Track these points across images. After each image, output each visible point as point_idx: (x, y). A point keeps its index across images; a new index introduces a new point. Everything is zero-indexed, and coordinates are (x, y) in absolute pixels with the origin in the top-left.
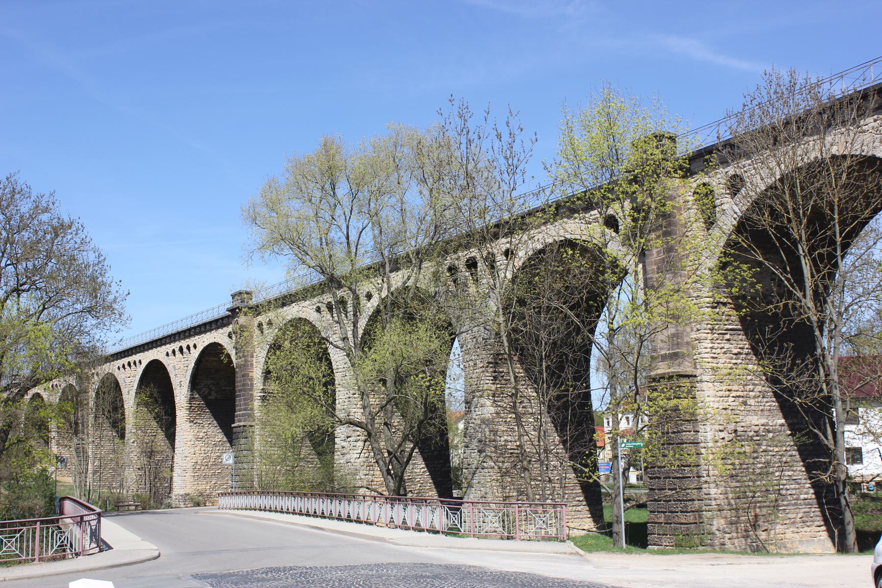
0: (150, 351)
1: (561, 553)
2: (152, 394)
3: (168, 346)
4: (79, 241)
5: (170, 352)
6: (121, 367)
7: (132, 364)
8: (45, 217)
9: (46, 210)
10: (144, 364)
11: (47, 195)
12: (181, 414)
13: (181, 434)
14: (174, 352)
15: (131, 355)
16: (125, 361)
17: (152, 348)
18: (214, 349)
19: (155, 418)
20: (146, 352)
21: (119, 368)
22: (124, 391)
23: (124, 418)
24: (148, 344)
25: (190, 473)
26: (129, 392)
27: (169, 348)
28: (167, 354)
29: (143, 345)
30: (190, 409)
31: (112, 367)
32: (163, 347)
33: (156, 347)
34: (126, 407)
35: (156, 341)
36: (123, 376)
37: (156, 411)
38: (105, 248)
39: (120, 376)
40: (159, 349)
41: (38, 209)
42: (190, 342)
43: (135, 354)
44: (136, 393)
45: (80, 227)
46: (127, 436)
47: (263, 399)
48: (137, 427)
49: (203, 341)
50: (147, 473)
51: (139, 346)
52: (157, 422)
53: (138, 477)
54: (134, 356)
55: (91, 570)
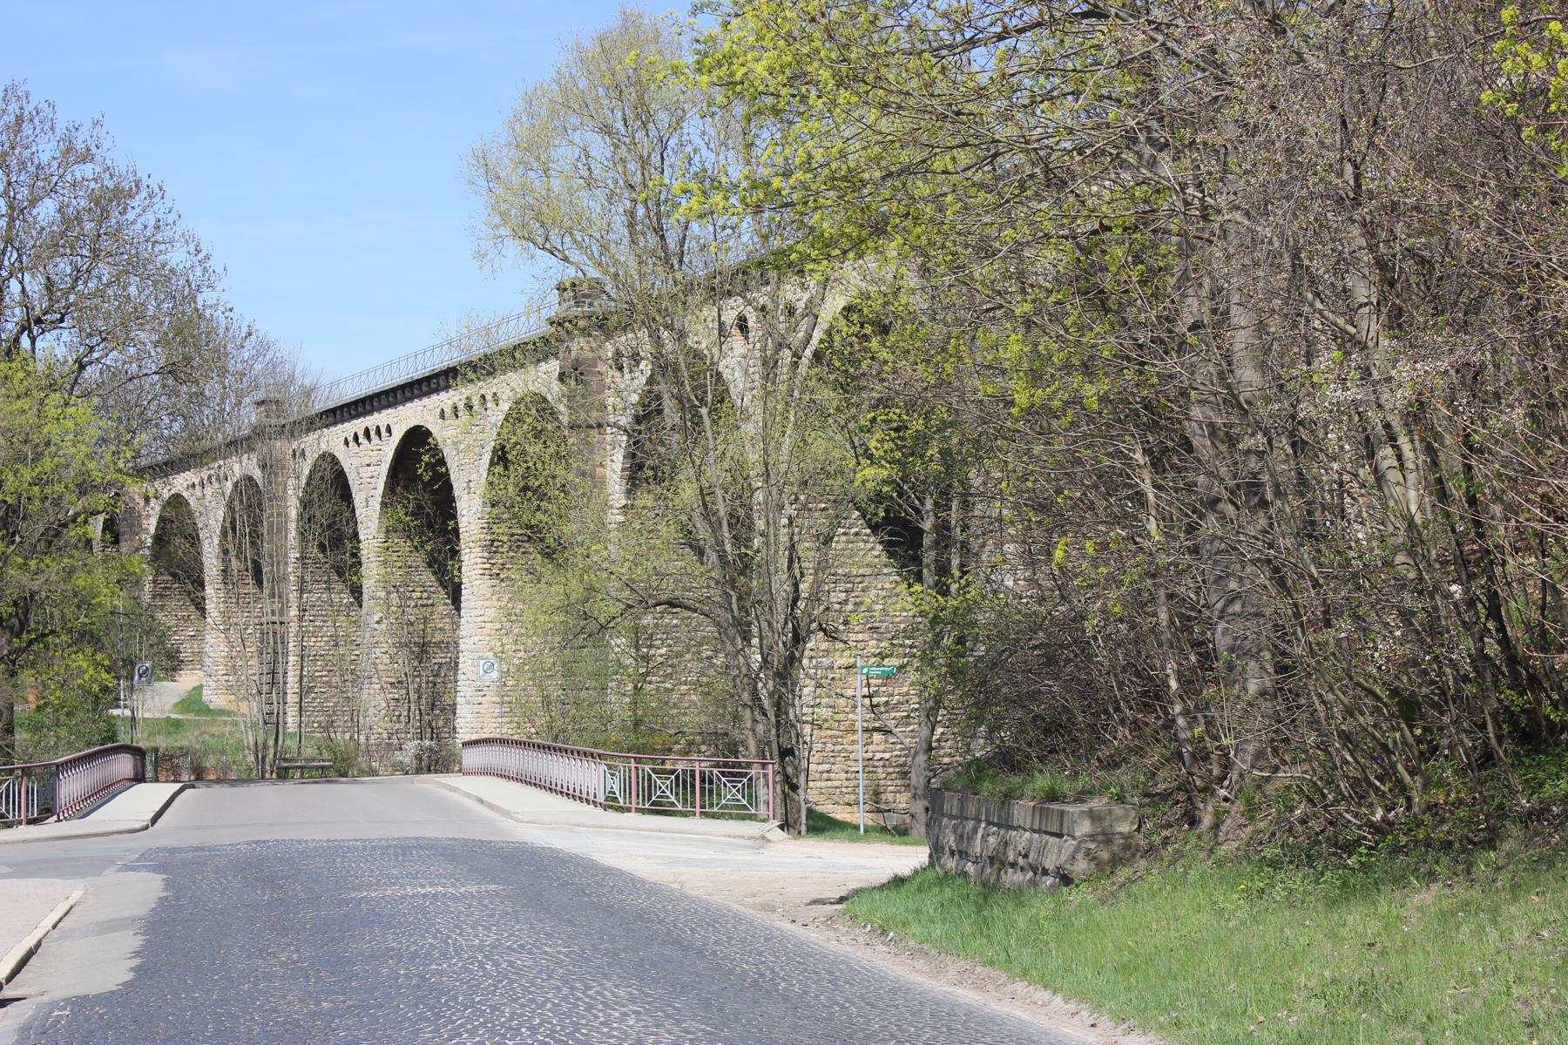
0: (409, 405)
1: (735, 837)
2: (420, 507)
3: (443, 395)
4: (152, 223)
5: (448, 411)
6: (350, 439)
7: (373, 433)
8: (88, 170)
9: (86, 157)
10: (398, 434)
11: (88, 125)
12: (472, 562)
13: (472, 604)
14: (356, 438)
15: (370, 412)
16: (358, 425)
17: (411, 399)
18: (417, 437)
19: (430, 565)
20: (400, 408)
21: (347, 443)
22: (358, 499)
23: (360, 564)
24: (402, 387)
25: (491, 697)
26: (367, 501)
27: (445, 399)
28: (442, 415)
29: (394, 390)
30: (492, 547)
31: (333, 439)
32: (434, 397)
33: (420, 397)
34: (362, 537)
35: (419, 382)
36: (356, 461)
37: (428, 548)
38: (209, 233)
39: (350, 461)
40: (425, 400)
41: (73, 154)
42: (488, 387)
43: (379, 410)
44: (384, 505)
45: (157, 190)
46: (365, 597)
47: (1157, 465)
48: (390, 587)
49: (402, 418)
50: (413, 696)
51: (386, 393)
52: (434, 573)
53: (393, 703)
54: (376, 415)
55: (24, 841)
